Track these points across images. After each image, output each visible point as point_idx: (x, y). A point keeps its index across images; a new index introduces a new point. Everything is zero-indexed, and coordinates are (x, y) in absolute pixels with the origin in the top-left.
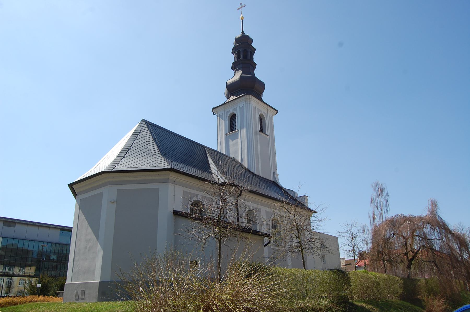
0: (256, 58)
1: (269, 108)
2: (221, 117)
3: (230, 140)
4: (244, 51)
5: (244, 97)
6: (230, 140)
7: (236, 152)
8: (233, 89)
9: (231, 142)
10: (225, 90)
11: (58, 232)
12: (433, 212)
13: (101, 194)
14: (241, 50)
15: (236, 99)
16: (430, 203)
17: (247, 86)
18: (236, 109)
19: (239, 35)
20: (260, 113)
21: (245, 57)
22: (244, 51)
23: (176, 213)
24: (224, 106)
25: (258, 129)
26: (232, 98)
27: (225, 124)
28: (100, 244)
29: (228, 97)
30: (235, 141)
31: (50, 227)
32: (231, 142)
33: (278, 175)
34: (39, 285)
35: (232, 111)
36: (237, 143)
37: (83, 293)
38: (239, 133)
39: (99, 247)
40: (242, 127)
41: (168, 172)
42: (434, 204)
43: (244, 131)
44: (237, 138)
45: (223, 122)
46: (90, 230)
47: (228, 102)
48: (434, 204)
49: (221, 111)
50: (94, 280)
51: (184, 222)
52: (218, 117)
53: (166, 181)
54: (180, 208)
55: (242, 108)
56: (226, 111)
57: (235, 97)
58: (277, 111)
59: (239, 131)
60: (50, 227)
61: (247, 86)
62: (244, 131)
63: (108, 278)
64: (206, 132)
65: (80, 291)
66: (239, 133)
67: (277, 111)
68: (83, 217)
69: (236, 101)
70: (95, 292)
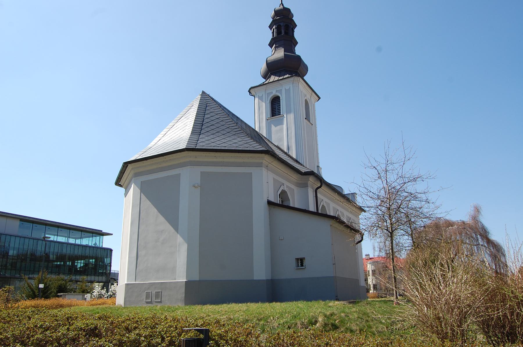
0: (298, 34)
1: (313, 93)
2: (260, 98)
3: (273, 126)
4: (283, 26)
5: (292, 79)
6: (273, 126)
7: (281, 139)
8: (273, 69)
9: (273, 128)
10: (264, 66)
11: (18, 222)
12: (475, 218)
13: (178, 176)
14: (282, 24)
15: (278, 80)
16: (473, 209)
17: (288, 66)
18: (280, 91)
19: (278, 7)
20: (305, 98)
21: (286, 33)
22: (283, 26)
23: (270, 203)
24: (265, 86)
25: (305, 117)
26: (273, 78)
27: (265, 108)
28: (180, 235)
29: (266, 76)
30: (278, 127)
31: (7, 217)
32: (273, 128)
33: (321, 169)
34: (41, 286)
35: (274, 93)
36: (282, 129)
37: (158, 295)
38: (285, 119)
39: (180, 239)
40: (288, 112)
41: (263, 155)
42: (477, 210)
43: (291, 116)
44: (282, 124)
45: (264, 104)
46: (161, 219)
47: (268, 83)
48: (477, 210)
49: (261, 92)
50: (175, 279)
51: (282, 214)
52: (257, 99)
53: (260, 165)
54: (272, 199)
55: (288, 91)
56: (267, 92)
57: (277, 78)
58: (319, 98)
59: (285, 116)
60: (7, 217)
61: (288, 66)
62: (291, 116)
63: (196, 278)
64: (252, 113)
65: (154, 292)
66: (285, 119)
67: (319, 98)
68: (147, 203)
69: (280, 82)
70: (181, 293)
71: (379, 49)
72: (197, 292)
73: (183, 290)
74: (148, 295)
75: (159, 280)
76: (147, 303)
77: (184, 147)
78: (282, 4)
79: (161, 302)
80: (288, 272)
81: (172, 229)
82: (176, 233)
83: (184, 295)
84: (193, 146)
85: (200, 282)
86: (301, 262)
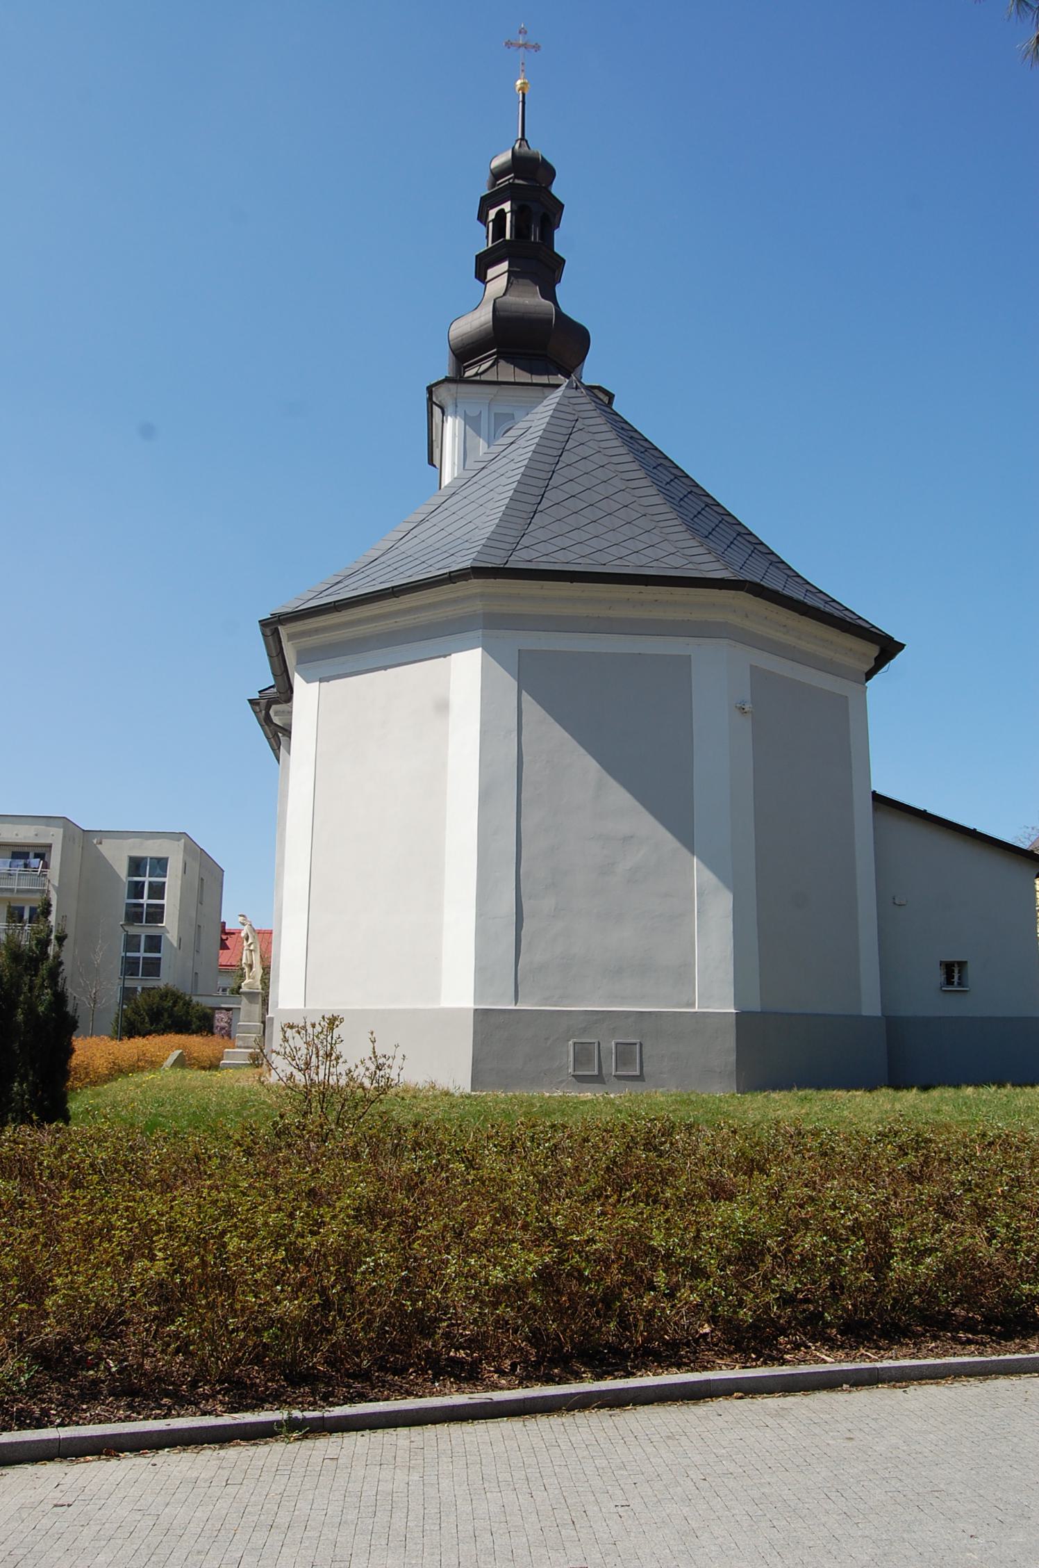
4: (524, 217)
22: (524, 217)
46: (619, 796)
63: (755, 1006)
68: (550, 735)
70: (725, 1051)
71: (148, 431)
72: (775, 1047)
73: (731, 1041)
74: (582, 1054)
75: (621, 1005)
76: (581, 1079)
77: (467, 564)
78: (523, 139)
79: (640, 1078)
80: (925, 999)
81: (668, 836)
82: (685, 852)
83: (733, 1058)
84: (496, 561)
85: (763, 1013)
86: (952, 971)
